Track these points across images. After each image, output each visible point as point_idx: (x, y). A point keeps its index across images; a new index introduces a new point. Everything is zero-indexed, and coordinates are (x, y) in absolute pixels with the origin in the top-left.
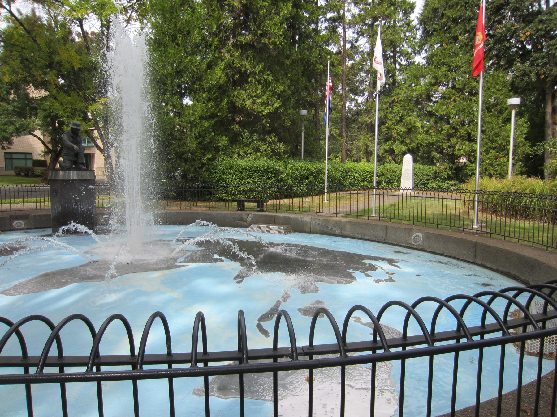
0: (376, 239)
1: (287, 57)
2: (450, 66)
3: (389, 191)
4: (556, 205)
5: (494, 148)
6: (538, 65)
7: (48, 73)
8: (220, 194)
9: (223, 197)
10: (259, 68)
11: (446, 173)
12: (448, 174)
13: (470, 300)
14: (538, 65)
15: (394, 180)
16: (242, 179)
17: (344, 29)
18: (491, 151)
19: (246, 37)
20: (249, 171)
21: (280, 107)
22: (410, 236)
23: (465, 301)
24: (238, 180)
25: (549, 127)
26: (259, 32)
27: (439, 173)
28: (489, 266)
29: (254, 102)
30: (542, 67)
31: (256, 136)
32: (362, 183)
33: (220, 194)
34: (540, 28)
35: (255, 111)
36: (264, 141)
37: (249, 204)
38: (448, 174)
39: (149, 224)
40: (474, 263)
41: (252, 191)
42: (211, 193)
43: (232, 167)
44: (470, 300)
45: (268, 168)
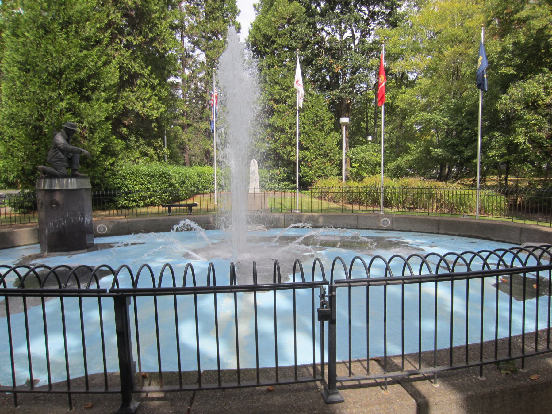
0: (349, 226)
1: (24, 44)
5: (320, 155)
6: (346, 92)
8: (122, 201)
9: (125, 204)
10: (146, 72)
13: (491, 253)
16: (142, 184)
17: (182, 37)
20: (148, 176)
21: (165, 111)
22: (379, 221)
23: (472, 255)
24: (139, 186)
26: (151, 35)
28: (451, 233)
29: (144, 106)
30: (349, 94)
31: (142, 141)
33: (122, 201)
35: (144, 115)
36: (150, 145)
37: (174, 208)
40: (438, 233)
41: (150, 197)
42: (111, 201)
43: (133, 172)
44: (491, 253)
45: (163, 173)
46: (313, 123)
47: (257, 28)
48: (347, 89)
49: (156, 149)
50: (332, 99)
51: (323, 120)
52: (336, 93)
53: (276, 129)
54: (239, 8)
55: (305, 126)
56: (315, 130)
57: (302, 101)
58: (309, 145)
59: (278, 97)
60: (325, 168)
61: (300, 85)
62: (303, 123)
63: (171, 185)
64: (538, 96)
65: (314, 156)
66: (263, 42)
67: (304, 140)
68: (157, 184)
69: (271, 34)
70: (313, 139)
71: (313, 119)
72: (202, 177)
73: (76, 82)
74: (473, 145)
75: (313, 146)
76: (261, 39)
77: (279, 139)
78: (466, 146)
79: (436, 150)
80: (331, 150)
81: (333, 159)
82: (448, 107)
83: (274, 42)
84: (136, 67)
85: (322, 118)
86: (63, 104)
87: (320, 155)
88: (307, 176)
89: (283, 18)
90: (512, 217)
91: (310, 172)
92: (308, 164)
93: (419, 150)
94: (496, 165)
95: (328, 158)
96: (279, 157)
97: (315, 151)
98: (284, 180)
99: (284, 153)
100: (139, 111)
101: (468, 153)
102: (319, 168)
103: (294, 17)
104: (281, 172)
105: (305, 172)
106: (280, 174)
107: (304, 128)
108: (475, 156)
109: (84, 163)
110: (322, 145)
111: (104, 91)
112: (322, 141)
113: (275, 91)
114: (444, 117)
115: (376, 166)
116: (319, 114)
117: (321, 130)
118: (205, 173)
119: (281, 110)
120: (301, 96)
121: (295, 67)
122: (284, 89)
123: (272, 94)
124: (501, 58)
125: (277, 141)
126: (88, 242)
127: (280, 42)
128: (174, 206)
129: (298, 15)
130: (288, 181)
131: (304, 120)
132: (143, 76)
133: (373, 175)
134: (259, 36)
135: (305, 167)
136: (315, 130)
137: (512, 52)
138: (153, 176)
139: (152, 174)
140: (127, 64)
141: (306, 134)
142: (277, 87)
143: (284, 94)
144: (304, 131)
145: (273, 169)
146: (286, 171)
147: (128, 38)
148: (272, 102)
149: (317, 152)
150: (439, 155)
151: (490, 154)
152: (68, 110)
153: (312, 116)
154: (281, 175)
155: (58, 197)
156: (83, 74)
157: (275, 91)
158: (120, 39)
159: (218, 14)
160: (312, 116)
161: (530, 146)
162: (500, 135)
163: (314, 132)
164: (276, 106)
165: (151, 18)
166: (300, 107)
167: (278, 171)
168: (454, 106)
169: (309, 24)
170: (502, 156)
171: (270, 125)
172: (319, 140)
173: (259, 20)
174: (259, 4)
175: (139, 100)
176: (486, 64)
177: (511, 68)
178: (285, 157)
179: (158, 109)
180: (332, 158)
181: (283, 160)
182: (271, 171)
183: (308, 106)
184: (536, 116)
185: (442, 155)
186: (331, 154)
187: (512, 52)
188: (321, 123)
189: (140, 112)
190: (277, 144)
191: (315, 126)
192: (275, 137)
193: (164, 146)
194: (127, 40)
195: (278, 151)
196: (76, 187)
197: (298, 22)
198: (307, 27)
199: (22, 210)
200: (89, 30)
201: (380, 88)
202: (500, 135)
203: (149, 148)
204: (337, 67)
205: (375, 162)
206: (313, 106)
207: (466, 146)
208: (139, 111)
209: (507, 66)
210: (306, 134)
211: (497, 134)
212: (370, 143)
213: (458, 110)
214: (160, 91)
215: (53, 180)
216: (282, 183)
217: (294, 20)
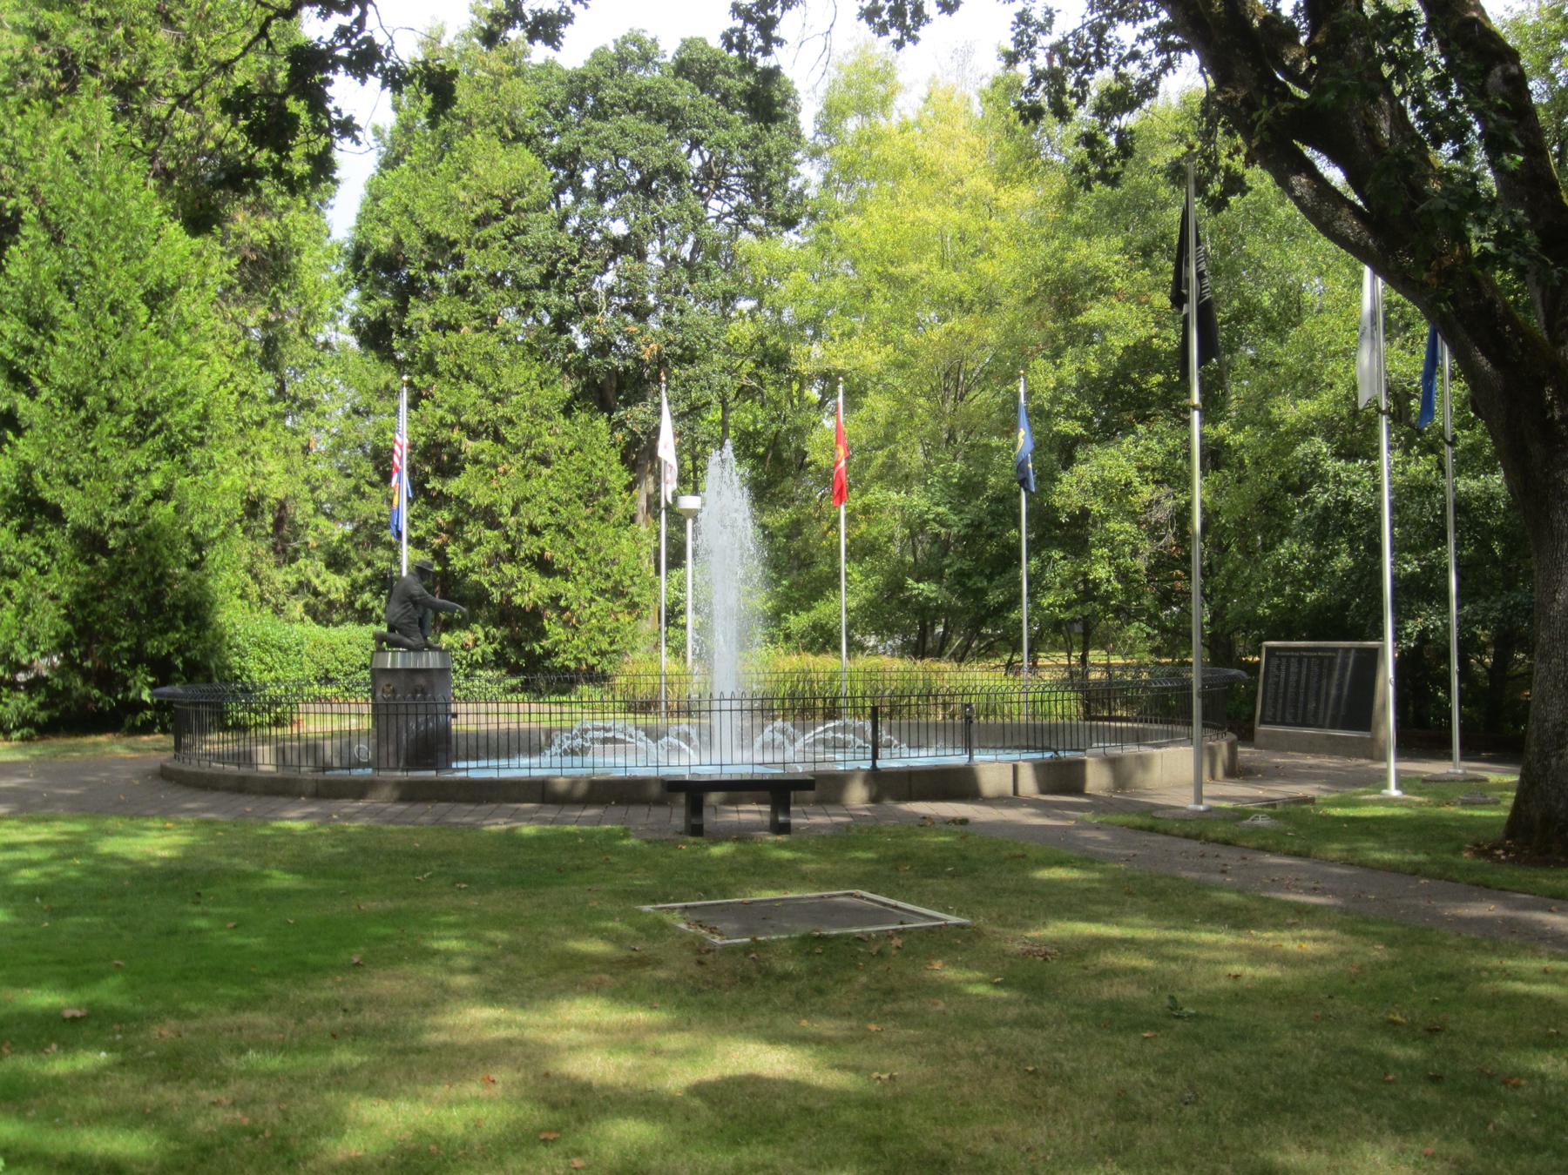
2: (485, 388)
5: (602, 592)
11: (478, 651)
38: (484, 652)
51: (606, 492)
52: (641, 416)
56: (587, 518)
60: (617, 630)
64: (1128, 484)
69: (454, 236)
70: (581, 545)
74: (1007, 576)
75: (583, 564)
78: (990, 578)
79: (921, 586)
82: (945, 477)
89: (493, 197)
93: (872, 582)
94: (1057, 626)
95: (626, 601)
98: (483, 665)
99: (492, 584)
101: (995, 597)
102: (602, 630)
104: (476, 640)
106: (476, 645)
108: (1013, 602)
114: (938, 505)
119: (484, 457)
124: (1055, 400)
130: (497, 666)
137: (1076, 390)
142: (472, 390)
143: (492, 413)
144: (551, 520)
146: (494, 638)
150: (928, 599)
151: (1045, 602)
162: (1064, 558)
163: (584, 525)
164: (470, 443)
168: (961, 478)
170: (1068, 606)
176: (1030, 447)
177: (1077, 424)
178: (496, 596)
184: (1127, 524)
185: (936, 599)
187: (1076, 390)
193: (850, 626)
199: (25, 731)
202: (1064, 558)
204: (648, 345)
207: (990, 578)
209: (1068, 417)
211: (1056, 554)
213: (968, 489)
216: (479, 672)
217: (522, 202)
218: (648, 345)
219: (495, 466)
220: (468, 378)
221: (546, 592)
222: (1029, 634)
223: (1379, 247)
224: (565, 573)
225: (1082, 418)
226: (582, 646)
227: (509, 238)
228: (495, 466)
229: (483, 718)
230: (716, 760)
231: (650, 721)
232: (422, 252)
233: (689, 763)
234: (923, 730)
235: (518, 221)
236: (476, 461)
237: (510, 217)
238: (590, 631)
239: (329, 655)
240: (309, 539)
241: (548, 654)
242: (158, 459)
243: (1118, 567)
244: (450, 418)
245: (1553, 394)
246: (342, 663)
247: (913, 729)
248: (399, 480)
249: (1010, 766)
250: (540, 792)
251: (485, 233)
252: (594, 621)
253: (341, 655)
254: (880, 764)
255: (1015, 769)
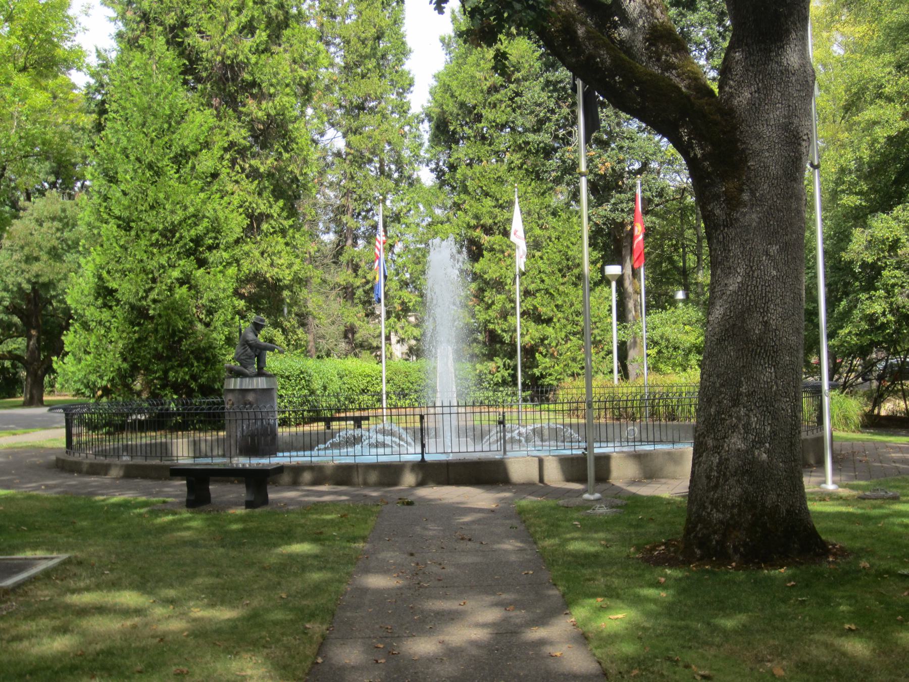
2: (497, 200)
3: (403, 410)
4: (676, 3)
5: (574, 334)
6: (622, 211)
7: (181, 234)
11: (499, 375)
12: (503, 376)
14: (622, 211)
15: (411, 390)
18: (572, 338)
19: (264, 164)
25: (630, 298)
27: (486, 374)
32: (361, 397)
34: (631, 203)
38: (503, 376)
39: (473, 356)
45: (302, 373)
46: (560, 271)
47: (445, 88)
48: (625, 205)
49: (284, 331)
50: (596, 224)
52: (603, 213)
53: (487, 283)
54: (410, 42)
55: (543, 276)
56: (563, 284)
57: (524, 259)
58: (551, 314)
59: (491, 221)
61: (519, 237)
62: (540, 272)
63: (312, 392)
65: (563, 334)
66: (458, 115)
67: (543, 305)
68: (294, 390)
70: (559, 302)
71: (559, 263)
72: (345, 379)
73: (192, 240)
75: (560, 315)
76: (455, 111)
77: (493, 303)
80: (595, 323)
81: (600, 341)
83: (479, 118)
84: (262, 206)
85: (577, 261)
86: (176, 274)
87: (574, 334)
88: (550, 375)
90: (699, 404)
91: (556, 367)
92: (551, 351)
96: (493, 338)
97: (565, 326)
100: (266, 272)
102: (574, 360)
103: (518, 71)
105: (546, 368)
107: (543, 281)
109: (202, 359)
110: (578, 314)
111: (225, 251)
112: (578, 306)
113: (484, 210)
115: (690, 351)
116: (570, 253)
117: (575, 285)
118: (350, 372)
119: (496, 247)
120: (521, 253)
121: (509, 221)
122: (501, 207)
123: (477, 217)
125: (489, 307)
126: (185, 482)
127: (491, 117)
128: (340, 419)
129: (526, 65)
131: (542, 266)
132: (269, 216)
133: (685, 370)
134: (451, 107)
135: (545, 356)
136: (563, 284)
138: (288, 377)
139: (287, 374)
140: (250, 203)
141: (547, 292)
142: (489, 202)
144: (542, 286)
145: (482, 363)
147: (253, 162)
148: (478, 233)
149: (569, 327)
152: (182, 282)
153: (557, 257)
154: (499, 375)
155: (251, 397)
156: (201, 229)
157: (484, 210)
158: (240, 166)
159: (371, 64)
160: (557, 257)
161: (893, 319)
163: (561, 288)
164: (487, 238)
165: (287, 131)
166: (520, 270)
167: (492, 365)
169: (548, 83)
171: (476, 277)
172: (572, 305)
173: (451, 74)
174: (450, 37)
175: (266, 255)
179: (290, 266)
180: (598, 338)
181: (502, 343)
182: (478, 366)
183: (550, 238)
186: (596, 332)
188: (576, 271)
189: (268, 275)
190: (490, 312)
191: (564, 276)
192: (486, 299)
194: (251, 166)
195: (491, 326)
196: (265, 387)
197: (525, 79)
198: (543, 89)
200: (206, 162)
201: (636, 242)
203: (275, 331)
204: (603, 164)
205: (688, 345)
206: (558, 238)
208: (266, 272)
210: (547, 292)
212: (681, 305)
214: (294, 237)
215: (244, 380)
218: (603, 164)
219: (503, 252)
220: (487, 194)
221: (537, 335)
222: (819, 353)
223: (595, 24)
224: (549, 321)
225: (860, 193)
226: (561, 370)
227: (511, 99)
228: (503, 252)
229: (477, 417)
230: (440, 450)
231: (288, 430)
232: (458, 115)
233: (384, 456)
234: (663, 429)
235: (517, 88)
236: (492, 250)
237: (512, 86)
238: (566, 360)
239: (403, 379)
240: (396, 305)
241: (542, 376)
242: (180, 259)
243: (891, 304)
244: (473, 222)
245: (689, 134)
246: (412, 383)
247: (650, 428)
248: (379, 264)
249: (537, 459)
250: (320, 474)
251: (493, 99)
252: (569, 353)
253: (412, 379)
254: (428, 458)
255: (541, 461)
